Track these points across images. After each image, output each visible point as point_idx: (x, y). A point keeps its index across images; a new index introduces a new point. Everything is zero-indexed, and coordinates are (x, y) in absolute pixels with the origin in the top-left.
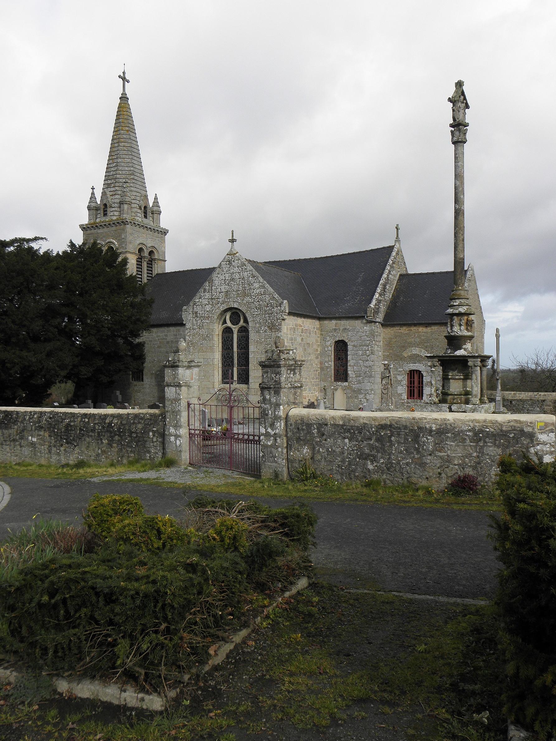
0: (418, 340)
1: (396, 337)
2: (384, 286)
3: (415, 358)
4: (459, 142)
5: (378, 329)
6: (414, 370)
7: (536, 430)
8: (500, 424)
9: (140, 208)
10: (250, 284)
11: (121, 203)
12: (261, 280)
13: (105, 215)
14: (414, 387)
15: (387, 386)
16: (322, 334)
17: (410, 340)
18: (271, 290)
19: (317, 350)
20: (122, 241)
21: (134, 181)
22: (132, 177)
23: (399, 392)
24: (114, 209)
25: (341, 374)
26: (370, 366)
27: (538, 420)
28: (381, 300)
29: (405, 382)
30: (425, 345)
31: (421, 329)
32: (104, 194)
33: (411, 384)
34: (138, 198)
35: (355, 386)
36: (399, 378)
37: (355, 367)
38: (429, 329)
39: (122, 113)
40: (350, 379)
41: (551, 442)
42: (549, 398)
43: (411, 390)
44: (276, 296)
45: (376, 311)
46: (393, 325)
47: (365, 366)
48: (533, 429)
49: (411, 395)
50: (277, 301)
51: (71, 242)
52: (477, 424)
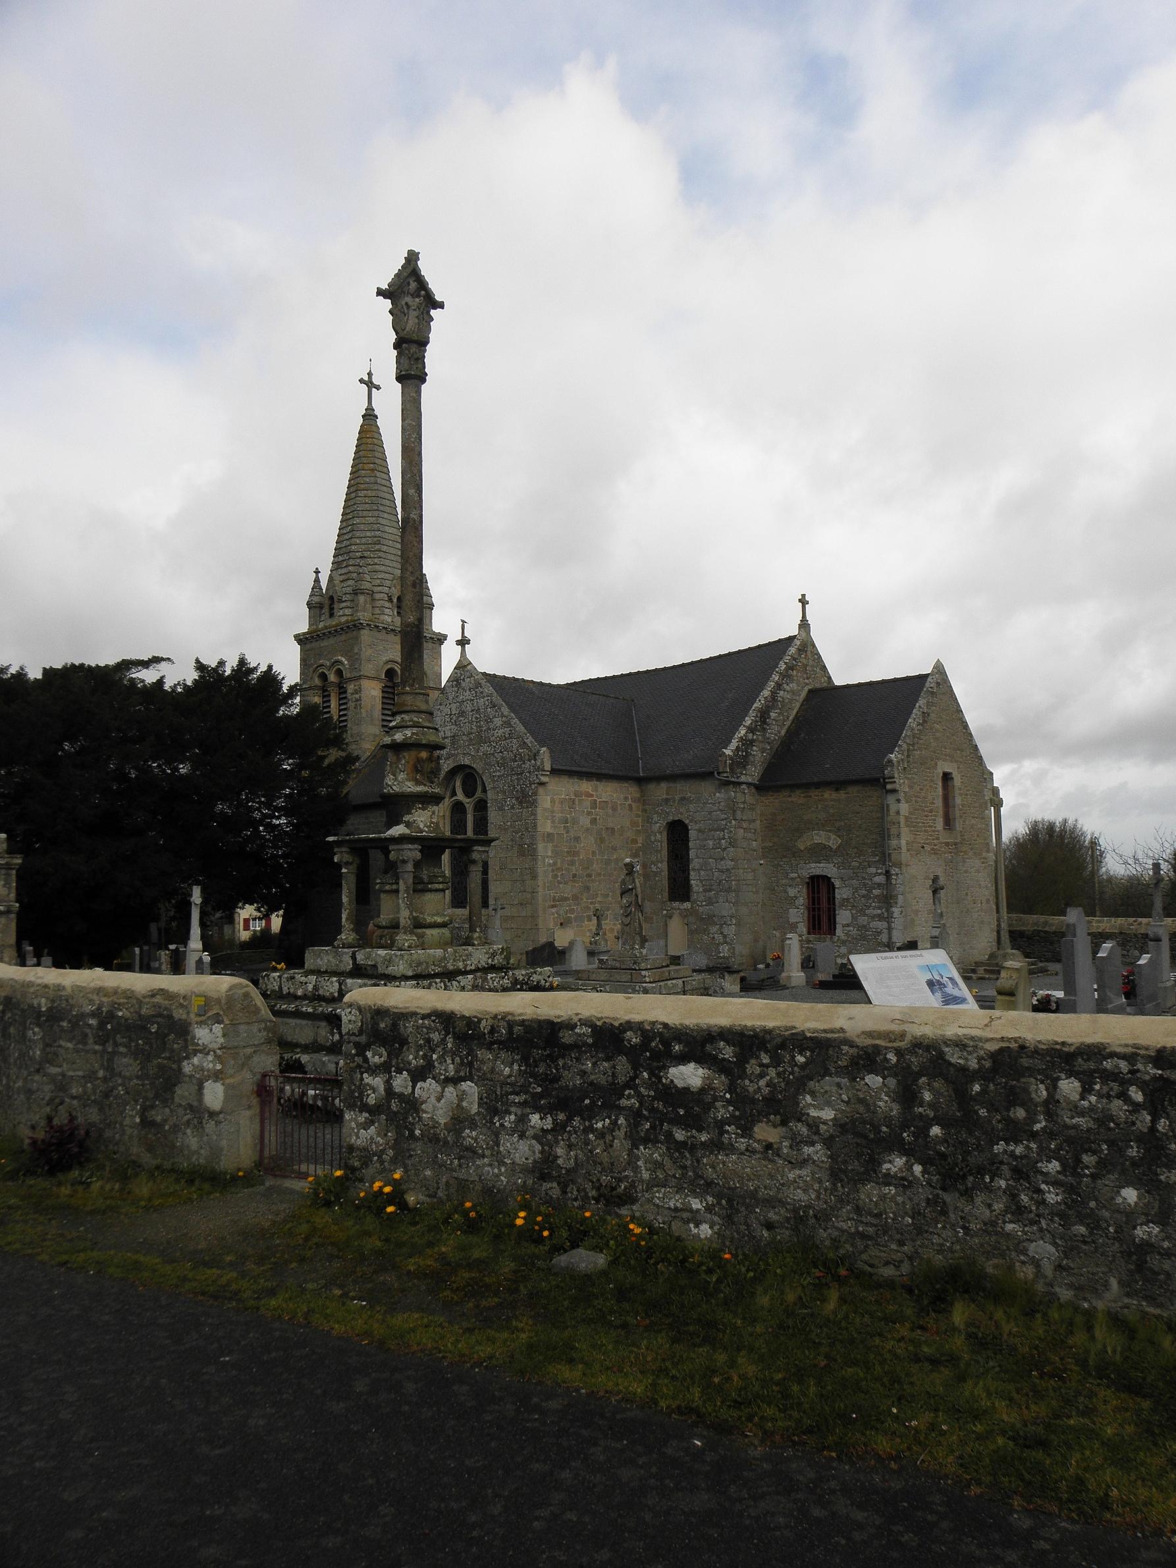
2: (764, 715)
3: (819, 853)
4: (411, 374)
5: (744, 797)
6: (818, 876)
7: (192, 1016)
8: (137, 999)
9: (390, 600)
10: (489, 720)
11: (356, 592)
12: (505, 710)
13: (331, 615)
14: (819, 909)
16: (644, 811)
18: (521, 728)
19: (635, 841)
20: (355, 659)
21: (381, 554)
22: (377, 547)
23: (792, 920)
24: (344, 604)
25: (679, 889)
27: (196, 990)
28: (752, 742)
29: (802, 901)
30: (837, 824)
31: (828, 794)
32: (331, 579)
33: (813, 904)
34: (388, 583)
35: (703, 910)
36: (792, 892)
37: (702, 873)
38: (842, 795)
39: (364, 440)
40: (694, 896)
41: (216, 1046)
43: (814, 916)
44: (529, 740)
45: (741, 761)
46: (778, 789)
48: (188, 1013)
50: (529, 748)
51: (197, 661)
52: (105, 999)
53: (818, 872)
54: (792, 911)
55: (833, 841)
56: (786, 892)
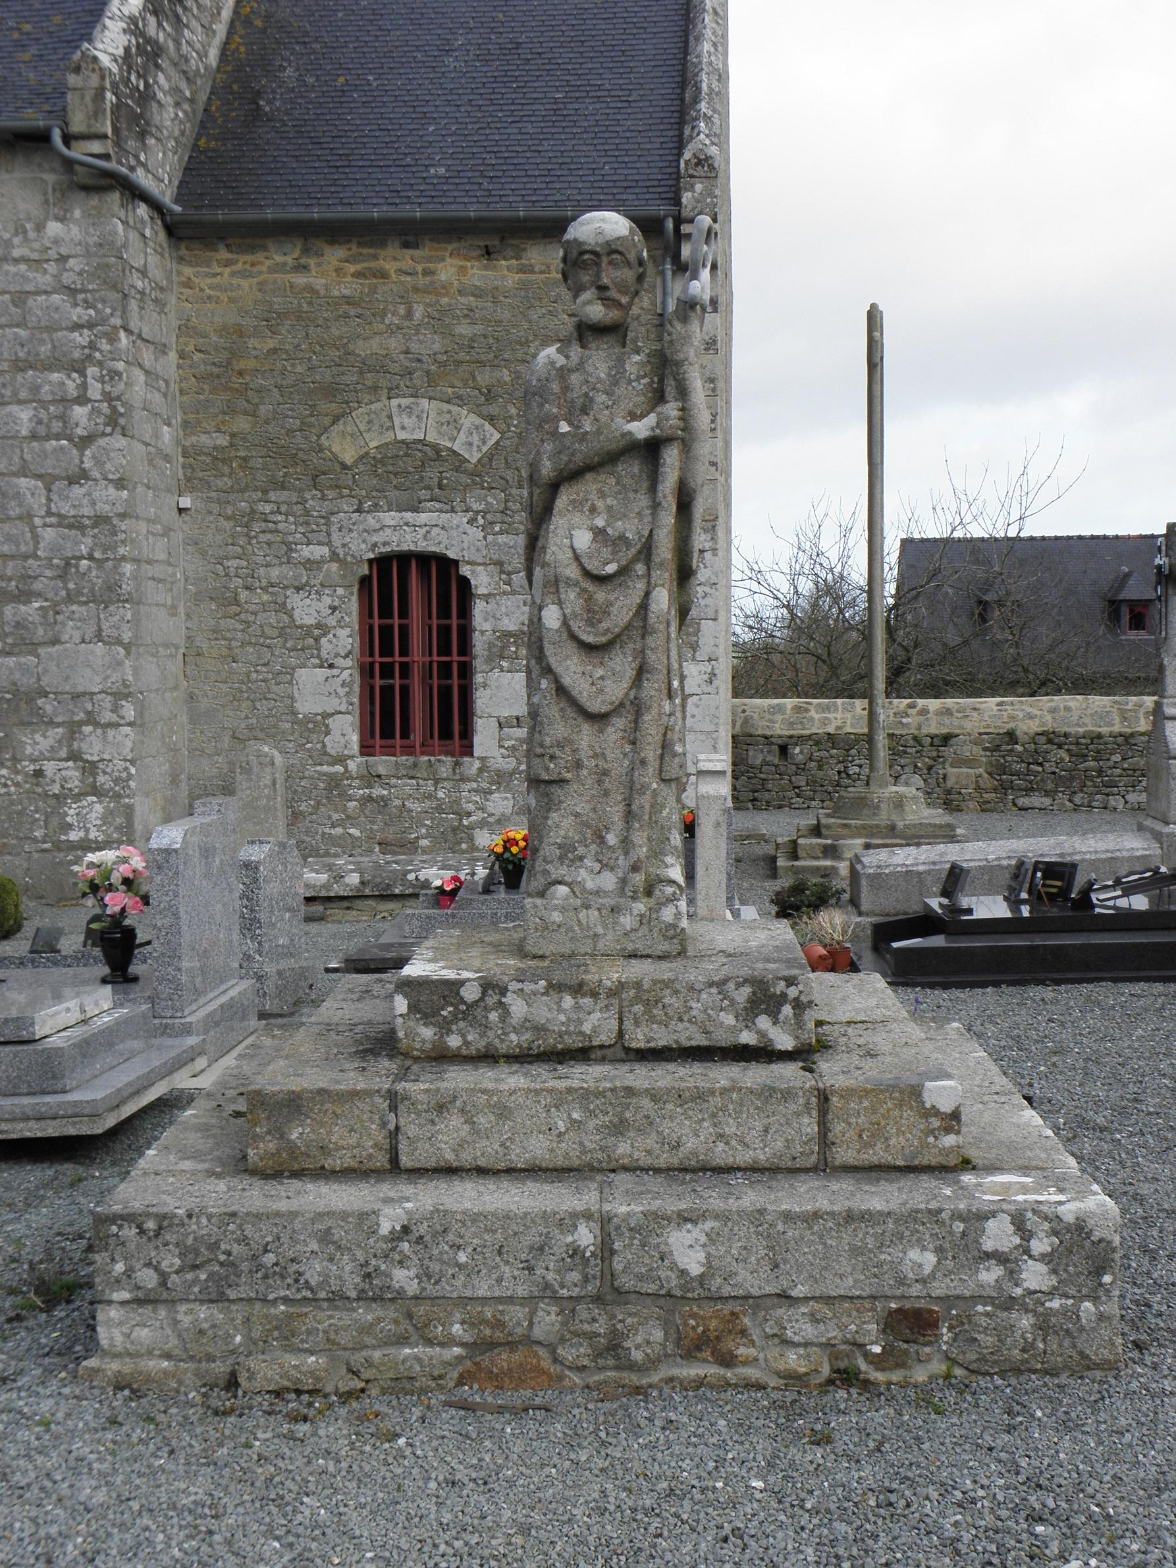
0: (430, 344)
1: (272, 320)
3: (416, 472)
5: (134, 235)
6: (404, 559)
14: (405, 669)
15: (621, 606)
17: (375, 344)
23: (307, 706)
26: (100, 520)
29: (344, 639)
30: (485, 377)
31: (454, 269)
42: (968, 725)
43: (387, 691)
47: (63, 522)
49: (385, 723)
53: (410, 542)
54: (309, 678)
55: (471, 436)
56: (282, 608)
